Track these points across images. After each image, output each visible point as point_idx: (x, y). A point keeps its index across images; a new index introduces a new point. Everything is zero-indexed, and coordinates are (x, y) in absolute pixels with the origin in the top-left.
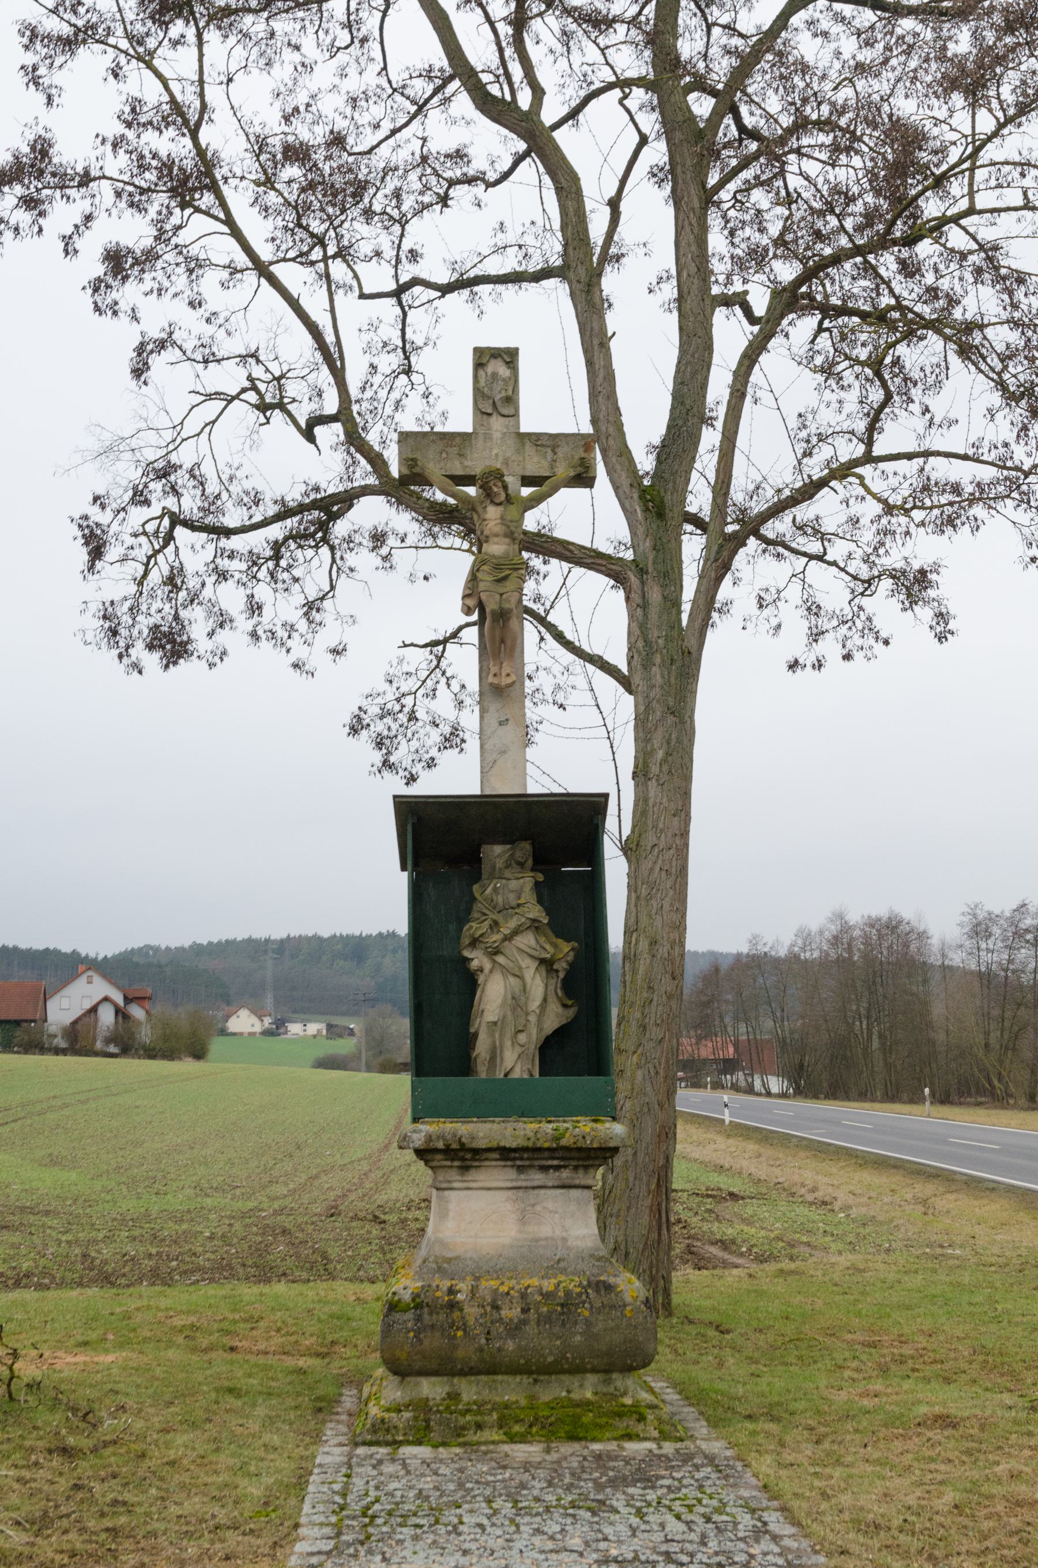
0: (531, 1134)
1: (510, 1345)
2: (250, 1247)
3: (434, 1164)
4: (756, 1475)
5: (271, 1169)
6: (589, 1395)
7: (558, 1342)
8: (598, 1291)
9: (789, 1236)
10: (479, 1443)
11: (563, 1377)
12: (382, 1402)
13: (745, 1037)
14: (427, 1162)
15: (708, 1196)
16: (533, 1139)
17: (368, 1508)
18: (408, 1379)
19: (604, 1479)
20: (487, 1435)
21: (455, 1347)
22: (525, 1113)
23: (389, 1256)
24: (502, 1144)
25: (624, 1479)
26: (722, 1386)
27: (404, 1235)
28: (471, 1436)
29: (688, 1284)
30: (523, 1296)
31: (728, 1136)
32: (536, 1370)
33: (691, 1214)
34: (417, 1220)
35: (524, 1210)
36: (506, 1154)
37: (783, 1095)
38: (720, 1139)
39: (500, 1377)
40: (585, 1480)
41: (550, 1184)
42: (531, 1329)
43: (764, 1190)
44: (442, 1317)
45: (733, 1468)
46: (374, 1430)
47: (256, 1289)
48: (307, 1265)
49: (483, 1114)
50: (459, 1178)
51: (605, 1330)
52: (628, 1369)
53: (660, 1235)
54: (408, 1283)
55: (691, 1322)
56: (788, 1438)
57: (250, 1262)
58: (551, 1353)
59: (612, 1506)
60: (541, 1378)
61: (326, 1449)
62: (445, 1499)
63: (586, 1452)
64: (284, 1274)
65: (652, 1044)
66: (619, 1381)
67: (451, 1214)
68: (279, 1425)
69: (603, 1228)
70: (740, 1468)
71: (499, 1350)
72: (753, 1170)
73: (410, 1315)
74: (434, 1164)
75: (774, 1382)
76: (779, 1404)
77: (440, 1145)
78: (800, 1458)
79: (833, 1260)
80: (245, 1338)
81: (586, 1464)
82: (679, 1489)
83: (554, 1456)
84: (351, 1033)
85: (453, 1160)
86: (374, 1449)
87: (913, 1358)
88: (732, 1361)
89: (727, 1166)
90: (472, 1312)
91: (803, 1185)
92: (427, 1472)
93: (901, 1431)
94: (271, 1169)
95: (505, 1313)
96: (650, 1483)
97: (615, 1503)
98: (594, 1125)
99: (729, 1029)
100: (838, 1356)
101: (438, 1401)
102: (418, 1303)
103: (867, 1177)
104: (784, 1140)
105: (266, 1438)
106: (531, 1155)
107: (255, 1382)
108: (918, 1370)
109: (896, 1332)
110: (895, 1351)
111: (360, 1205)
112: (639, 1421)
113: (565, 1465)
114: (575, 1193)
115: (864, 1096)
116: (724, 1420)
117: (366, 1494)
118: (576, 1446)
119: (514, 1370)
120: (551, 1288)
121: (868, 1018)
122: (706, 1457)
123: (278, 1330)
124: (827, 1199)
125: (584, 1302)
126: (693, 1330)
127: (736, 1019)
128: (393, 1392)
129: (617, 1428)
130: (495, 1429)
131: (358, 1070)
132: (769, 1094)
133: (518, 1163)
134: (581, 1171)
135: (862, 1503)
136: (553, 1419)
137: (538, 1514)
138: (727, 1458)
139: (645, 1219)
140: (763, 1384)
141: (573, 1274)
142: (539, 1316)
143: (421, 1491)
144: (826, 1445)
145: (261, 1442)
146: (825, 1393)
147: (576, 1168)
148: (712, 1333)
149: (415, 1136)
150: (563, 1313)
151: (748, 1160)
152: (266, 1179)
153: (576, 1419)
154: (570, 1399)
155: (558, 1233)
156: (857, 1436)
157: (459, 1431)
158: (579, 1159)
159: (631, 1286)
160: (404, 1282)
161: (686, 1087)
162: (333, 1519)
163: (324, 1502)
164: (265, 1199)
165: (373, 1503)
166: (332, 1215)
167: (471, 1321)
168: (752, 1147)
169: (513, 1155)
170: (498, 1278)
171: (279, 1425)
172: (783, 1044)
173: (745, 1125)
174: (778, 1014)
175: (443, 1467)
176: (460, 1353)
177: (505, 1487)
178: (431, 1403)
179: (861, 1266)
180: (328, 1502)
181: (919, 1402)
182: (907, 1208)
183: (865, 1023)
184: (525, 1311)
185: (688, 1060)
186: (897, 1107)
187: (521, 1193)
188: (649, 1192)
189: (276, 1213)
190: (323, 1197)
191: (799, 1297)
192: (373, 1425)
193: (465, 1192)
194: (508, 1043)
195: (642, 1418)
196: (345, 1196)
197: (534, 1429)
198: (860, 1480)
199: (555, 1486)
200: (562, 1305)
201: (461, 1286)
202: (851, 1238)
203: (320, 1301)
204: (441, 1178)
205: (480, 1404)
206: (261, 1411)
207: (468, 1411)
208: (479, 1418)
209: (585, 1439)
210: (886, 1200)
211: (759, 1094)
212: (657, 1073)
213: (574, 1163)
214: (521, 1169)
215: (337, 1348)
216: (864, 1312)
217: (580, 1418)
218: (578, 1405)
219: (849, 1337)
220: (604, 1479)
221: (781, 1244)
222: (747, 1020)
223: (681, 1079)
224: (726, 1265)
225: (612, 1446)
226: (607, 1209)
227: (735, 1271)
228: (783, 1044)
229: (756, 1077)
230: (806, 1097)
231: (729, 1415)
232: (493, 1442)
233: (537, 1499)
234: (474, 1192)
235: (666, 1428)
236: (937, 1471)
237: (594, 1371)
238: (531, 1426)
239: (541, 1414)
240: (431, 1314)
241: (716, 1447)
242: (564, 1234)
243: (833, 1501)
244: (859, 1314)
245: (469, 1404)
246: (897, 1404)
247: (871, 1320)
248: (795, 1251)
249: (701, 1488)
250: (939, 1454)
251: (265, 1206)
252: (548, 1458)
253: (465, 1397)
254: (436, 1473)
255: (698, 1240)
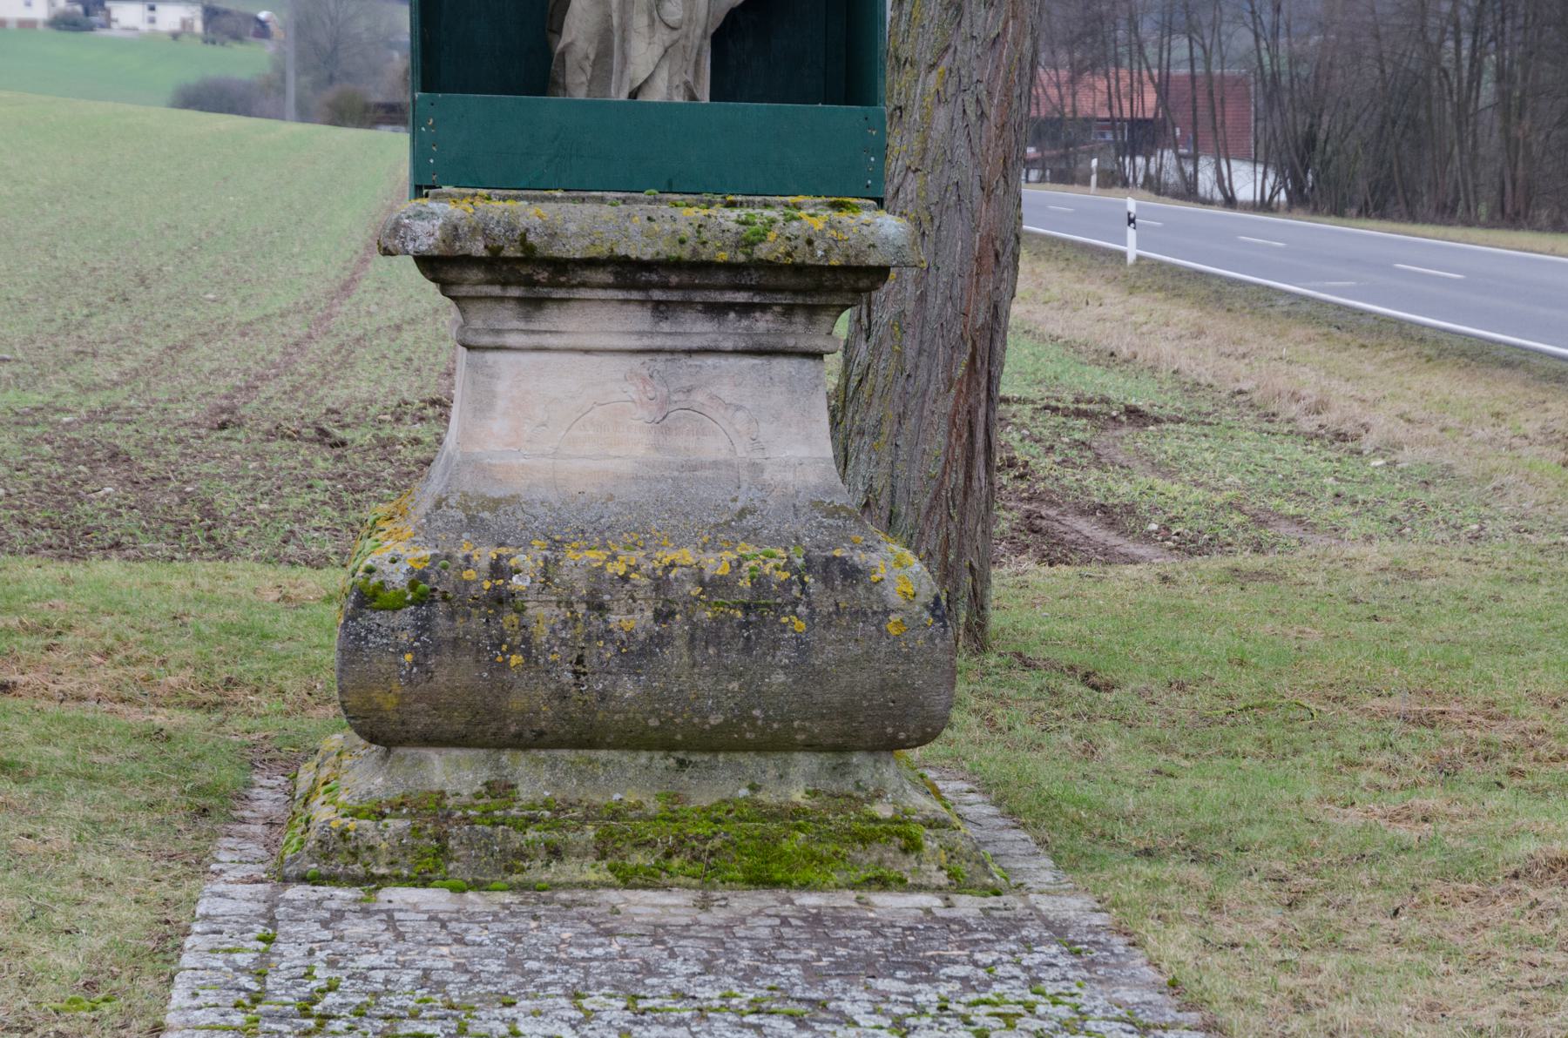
0: (687, 231)
1: (628, 688)
2: (37, 485)
3: (463, 291)
4: (1154, 964)
5: (80, 325)
6: (798, 796)
7: (734, 686)
8: (827, 580)
9: (1255, 503)
10: (555, 886)
11: (742, 758)
12: (342, 798)
13: (1184, 71)
14: (445, 286)
15: (1079, 414)
16: (691, 242)
17: (314, 1002)
18: (400, 751)
19: (825, 961)
20: (570, 870)
21: (507, 688)
22: (674, 183)
23: (352, 515)
24: (621, 251)
25: (870, 962)
26: (1091, 792)
27: (388, 472)
28: (537, 872)
29: (1023, 592)
30: (660, 584)
31: (1132, 290)
32: (683, 740)
33: (1037, 449)
34: (416, 441)
35: (667, 400)
36: (629, 274)
37: (1264, 206)
38: (1112, 295)
39: (603, 754)
40: (785, 962)
41: (729, 345)
42: (676, 656)
43: (1206, 407)
44: (477, 623)
45: (1105, 947)
46: (325, 850)
47: (55, 570)
48: (169, 528)
49: (579, 186)
50: (522, 325)
51: (841, 662)
52: (889, 745)
53: (969, 477)
54: (401, 549)
55: (1028, 665)
56: (1228, 895)
57: (38, 517)
58: (718, 706)
59: (840, 1013)
60: (695, 758)
61: (220, 887)
62: (479, 988)
63: (787, 910)
64: (117, 545)
65: (974, 48)
66: (864, 768)
67: (501, 404)
68: (115, 838)
69: (844, 459)
70: (1120, 949)
71: (603, 696)
72: (1183, 363)
73: (405, 617)
74: (463, 291)
75: (1202, 789)
76: (1214, 830)
77: (478, 248)
78: (1252, 934)
79: (1352, 552)
80: (33, 665)
81: (786, 931)
82: (988, 985)
83: (718, 915)
84: (262, 30)
85: (505, 284)
86: (324, 891)
87: (1513, 749)
88: (1113, 744)
89: (1125, 352)
90: (543, 616)
91: (1295, 397)
92: (442, 936)
93: (1474, 887)
94: (80, 325)
95: (618, 619)
96: (926, 971)
97: (847, 1007)
98: (835, 215)
99: (1151, 52)
100: (1350, 743)
101: (465, 800)
102: (424, 594)
103: (1442, 383)
104: (1261, 301)
105: (87, 861)
106: (685, 278)
107: (59, 752)
108: (1521, 773)
109: (1480, 695)
110: (1476, 733)
111: (288, 408)
112: (905, 851)
113: (740, 931)
114: (783, 366)
115: (1448, 212)
116: (1092, 857)
117: (309, 975)
118: (767, 898)
119: (634, 740)
120: (724, 570)
121: (1476, 32)
122: (1048, 925)
123: (107, 653)
124: (1348, 427)
125: (795, 603)
126: (1033, 680)
127: (1168, 29)
128: (365, 776)
129: (856, 864)
130: (591, 860)
131: (279, 115)
132: (1230, 202)
133: (657, 295)
134: (800, 319)
135: (1378, 1019)
136: (717, 842)
137: (680, 1023)
138: (1092, 929)
139: (937, 442)
140: (1180, 792)
141: (773, 541)
142: (694, 626)
143: (427, 972)
144: (1311, 909)
145: (77, 868)
146: (1315, 811)
147: (789, 310)
148: (1073, 687)
149: (419, 227)
150: (746, 625)
151: (1170, 344)
152: (68, 346)
153: (768, 844)
154: (757, 805)
155: (742, 452)
156: (1379, 896)
157: (513, 860)
158: (796, 292)
159: (900, 572)
160: (391, 547)
161: (1041, 180)
162: (238, 1019)
163: (216, 986)
164: (68, 388)
165: (323, 992)
166: (223, 426)
167: (541, 634)
168: (1184, 314)
169: (644, 277)
170: (604, 546)
171: (115, 838)
172: (1272, 87)
173: (1173, 267)
174: (1267, 18)
175: (476, 928)
176: (516, 702)
177: (611, 970)
178: (451, 802)
179: (1413, 566)
180: (227, 986)
181: (1518, 832)
182: (1526, 452)
183: (1467, 42)
184: (662, 616)
185: (1049, 121)
186: (1525, 237)
187: (660, 362)
188: (950, 383)
189: (93, 416)
190: (200, 389)
191: (1270, 623)
192: (322, 843)
193: (534, 356)
194: (640, 21)
195: (912, 846)
196: (250, 388)
197: (676, 862)
198: (1379, 978)
199: (719, 972)
200: (746, 608)
201: (520, 559)
202: (1395, 509)
203: (199, 600)
204: (477, 323)
205: (559, 809)
206: (73, 809)
207: (533, 820)
208: (555, 836)
209: (788, 884)
210: (1479, 434)
211: (1209, 202)
212: (982, 115)
213: (786, 299)
214: (661, 309)
215: (238, 694)
216: (1413, 655)
217: (776, 842)
218: (773, 817)
219: (1378, 703)
220: (825, 961)
221: (1238, 518)
222: (1191, 31)
223: (1030, 164)
224: (1109, 556)
225: (846, 899)
226: (854, 419)
227: (1130, 570)
228: (1272, 87)
229: (1203, 162)
230: (1316, 211)
231: (1102, 848)
232: (585, 885)
233: (680, 995)
234: (555, 357)
235: (964, 867)
236: (1545, 964)
237: (811, 747)
238: (668, 856)
239: (692, 831)
240: (451, 616)
241: (1072, 907)
242: (757, 456)
243: (1319, 1014)
244: (1401, 659)
245: (533, 806)
246: (1471, 836)
247: (1428, 672)
248: (1267, 534)
249: (1034, 983)
250: (1554, 933)
251: (70, 401)
252: (704, 918)
253: (525, 792)
254: (460, 941)
255: (1052, 503)
